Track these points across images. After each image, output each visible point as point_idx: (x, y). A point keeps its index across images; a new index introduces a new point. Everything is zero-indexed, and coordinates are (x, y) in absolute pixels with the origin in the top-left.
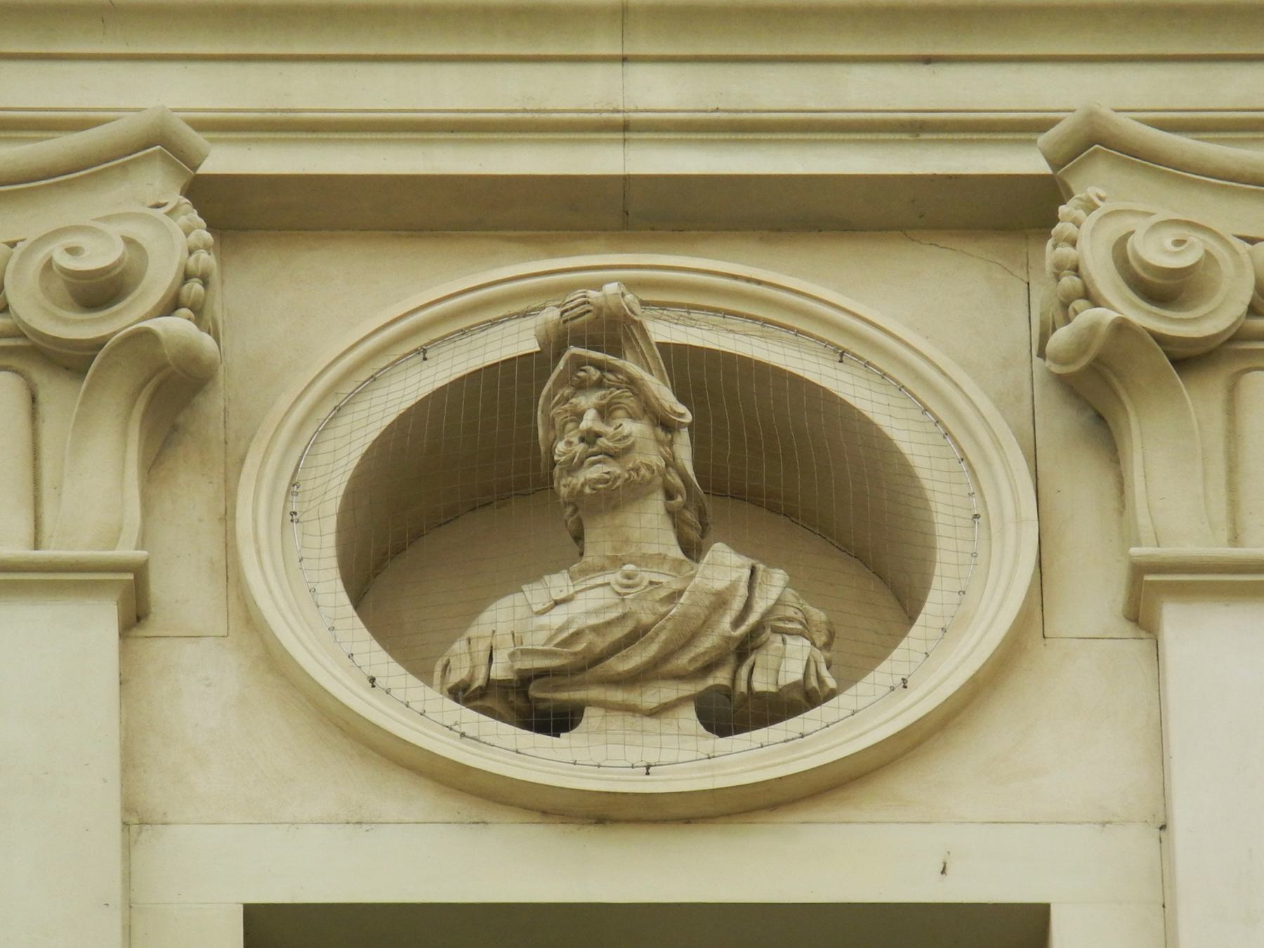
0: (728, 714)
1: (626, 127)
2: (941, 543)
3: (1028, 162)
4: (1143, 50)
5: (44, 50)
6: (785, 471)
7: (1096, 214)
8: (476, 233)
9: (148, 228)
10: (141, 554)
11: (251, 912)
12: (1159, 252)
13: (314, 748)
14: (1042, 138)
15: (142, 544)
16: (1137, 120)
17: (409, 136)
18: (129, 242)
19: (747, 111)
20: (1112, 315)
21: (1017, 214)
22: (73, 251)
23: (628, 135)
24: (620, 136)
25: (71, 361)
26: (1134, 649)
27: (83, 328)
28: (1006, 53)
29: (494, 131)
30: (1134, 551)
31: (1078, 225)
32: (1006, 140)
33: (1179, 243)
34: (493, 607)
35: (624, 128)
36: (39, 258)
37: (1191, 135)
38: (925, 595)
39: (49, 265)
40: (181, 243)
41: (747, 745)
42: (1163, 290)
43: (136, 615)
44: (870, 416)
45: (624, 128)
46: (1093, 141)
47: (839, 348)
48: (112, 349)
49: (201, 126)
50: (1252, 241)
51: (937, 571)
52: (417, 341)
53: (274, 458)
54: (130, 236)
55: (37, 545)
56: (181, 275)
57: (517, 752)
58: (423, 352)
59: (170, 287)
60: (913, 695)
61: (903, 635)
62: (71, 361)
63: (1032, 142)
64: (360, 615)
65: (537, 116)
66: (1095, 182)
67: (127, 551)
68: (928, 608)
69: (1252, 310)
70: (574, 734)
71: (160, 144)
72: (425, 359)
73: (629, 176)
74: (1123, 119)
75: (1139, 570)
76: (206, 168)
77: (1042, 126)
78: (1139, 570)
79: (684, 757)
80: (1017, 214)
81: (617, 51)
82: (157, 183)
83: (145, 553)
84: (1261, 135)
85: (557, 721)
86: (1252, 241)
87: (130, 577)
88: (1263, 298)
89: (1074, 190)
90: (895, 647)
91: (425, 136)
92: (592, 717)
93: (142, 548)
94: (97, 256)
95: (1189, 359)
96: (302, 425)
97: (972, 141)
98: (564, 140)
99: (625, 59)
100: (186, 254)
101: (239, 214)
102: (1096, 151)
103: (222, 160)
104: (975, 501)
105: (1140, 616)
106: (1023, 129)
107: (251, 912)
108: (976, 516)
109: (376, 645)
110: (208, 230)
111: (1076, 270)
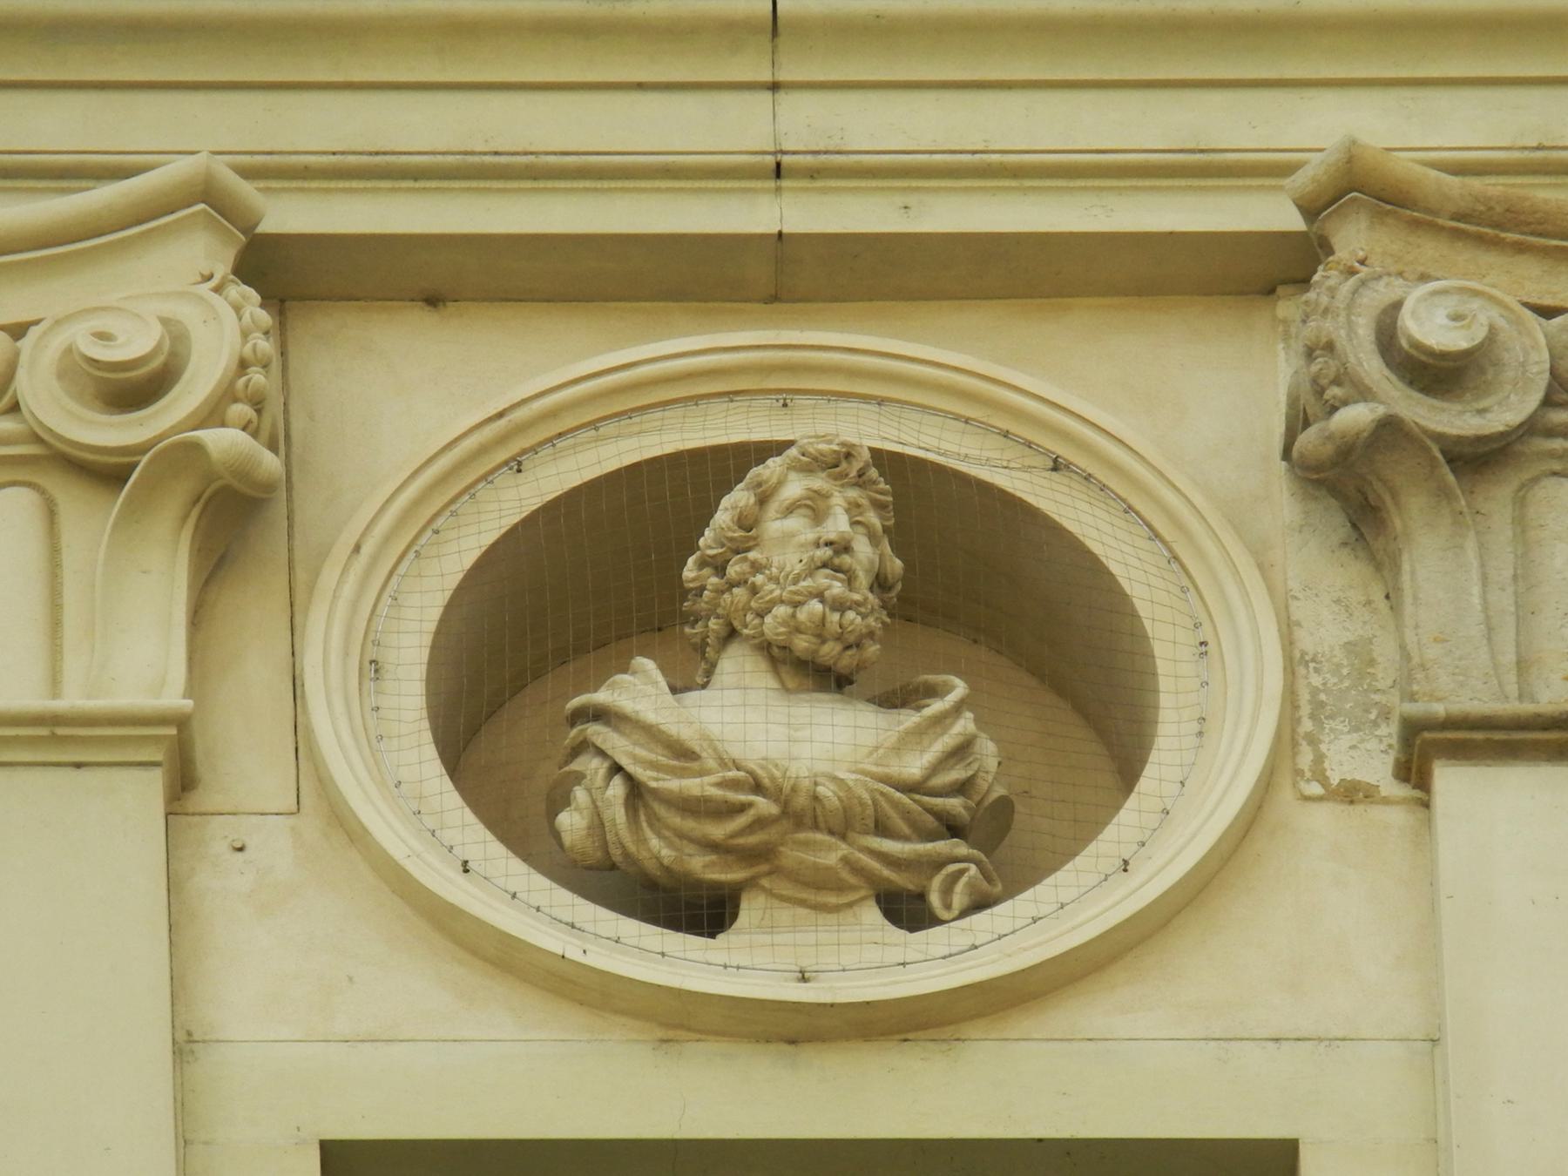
2: (1164, 683)
3: (1274, 214)
4: (1341, 73)
5: (1207, 76)
6: (984, 593)
8: (711, 305)
10: (188, 704)
12: (1433, 327)
13: (383, 938)
14: (1287, 182)
15: (189, 692)
18: (165, 322)
20: (1381, 410)
21: (1272, 272)
22: (103, 337)
25: (106, 473)
28: (1522, 74)
32: (1179, 188)
33: (1456, 317)
36: (58, 342)
39: (69, 351)
42: (1437, 374)
43: (183, 782)
46: (1357, 188)
50: (1547, 312)
52: (511, 443)
53: (348, 590)
54: (165, 315)
55: (55, 693)
56: (234, 366)
57: (573, 926)
59: (220, 382)
60: (1137, 875)
61: (1118, 808)
62: (106, 473)
63: (1281, 188)
65: (440, 158)
67: (173, 699)
69: (1548, 402)
72: (519, 471)
75: (1412, 730)
76: (267, 226)
77: (1285, 170)
78: (1412, 730)
79: (869, 961)
81: (766, 77)
82: (202, 252)
85: (707, 912)
86: (1547, 312)
87: (173, 731)
88: (1563, 388)
89: (1336, 247)
90: (1106, 824)
92: (751, 910)
94: (134, 342)
95: (1476, 460)
100: (238, 339)
102: (1354, 200)
103: (289, 215)
106: (1272, 171)
110: (262, 306)
111: (1330, 347)
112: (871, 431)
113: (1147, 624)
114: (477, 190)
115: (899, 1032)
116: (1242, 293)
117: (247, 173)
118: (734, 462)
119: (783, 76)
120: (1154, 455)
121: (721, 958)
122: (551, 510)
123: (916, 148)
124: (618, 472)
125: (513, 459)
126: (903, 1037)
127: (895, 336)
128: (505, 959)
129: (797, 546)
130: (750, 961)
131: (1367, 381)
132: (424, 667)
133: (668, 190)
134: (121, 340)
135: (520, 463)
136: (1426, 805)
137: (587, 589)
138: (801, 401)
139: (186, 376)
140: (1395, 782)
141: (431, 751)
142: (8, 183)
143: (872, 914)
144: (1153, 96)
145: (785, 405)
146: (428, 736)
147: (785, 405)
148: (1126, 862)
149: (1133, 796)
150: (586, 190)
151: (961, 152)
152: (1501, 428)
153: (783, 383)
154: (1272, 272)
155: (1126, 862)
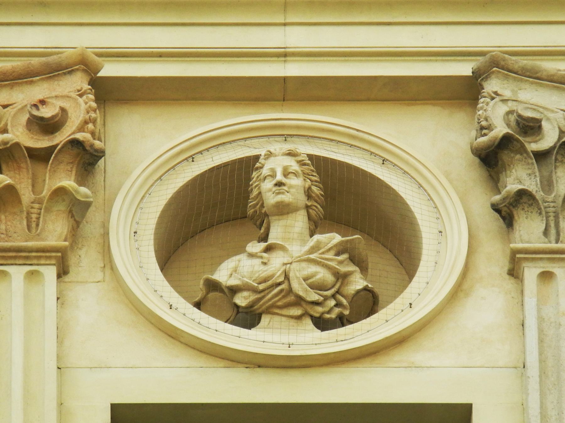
0: (322, 324)
1: (285, 55)
3: (464, 69)
6: (354, 206)
8: (204, 102)
9: (69, 98)
11: (115, 408)
21: (465, 93)
24: (283, 59)
25: (40, 156)
26: (509, 284)
27: (42, 143)
30: (512, 245)
31: (487, 104)
34: (227, 261)
35: (284, 55)
40: (83, 107)
44: (390, 184)
45: (284, 55)
47: (382, 157)
48: (60, 150)
49: (100, 55)
58: (192, 158)
60: (415, 309)
64: (165, 275)
65: (45, 50)
66: (492, 85)
68: (420, 269)
71: (85, 65)
72: (193, 161)
73: (287, 77)
75: (514, 252)
81: (283, 21)
82: (79, 81)
85: (248, 318)
87: (59, 254)
96: (147, 179)
99: (285, 24)
101: (110, 94)
103: (110, 70)
105: (514, 272)
107: (115, 408)
109: (172, 290)
112: (306, 149)
115: (246, 363)
116: (449, 99)
117: (100, 55)
119: (288, 21)
120: (424, 161)
123: (505, 45)
125: (191, 156)
126: (248, 366)
128: (173, 334)
130: (273, 337)
131: (57, 134)
132: (154, 230)
134: (25, 117)
135: (193, 158)
142: (2, 59)
144: (272, 28)
148: (411, 304)
150: (135, 61)
151: (519, 47)
152: (547, 148)
154: (465, 93)
155: (411, 304)
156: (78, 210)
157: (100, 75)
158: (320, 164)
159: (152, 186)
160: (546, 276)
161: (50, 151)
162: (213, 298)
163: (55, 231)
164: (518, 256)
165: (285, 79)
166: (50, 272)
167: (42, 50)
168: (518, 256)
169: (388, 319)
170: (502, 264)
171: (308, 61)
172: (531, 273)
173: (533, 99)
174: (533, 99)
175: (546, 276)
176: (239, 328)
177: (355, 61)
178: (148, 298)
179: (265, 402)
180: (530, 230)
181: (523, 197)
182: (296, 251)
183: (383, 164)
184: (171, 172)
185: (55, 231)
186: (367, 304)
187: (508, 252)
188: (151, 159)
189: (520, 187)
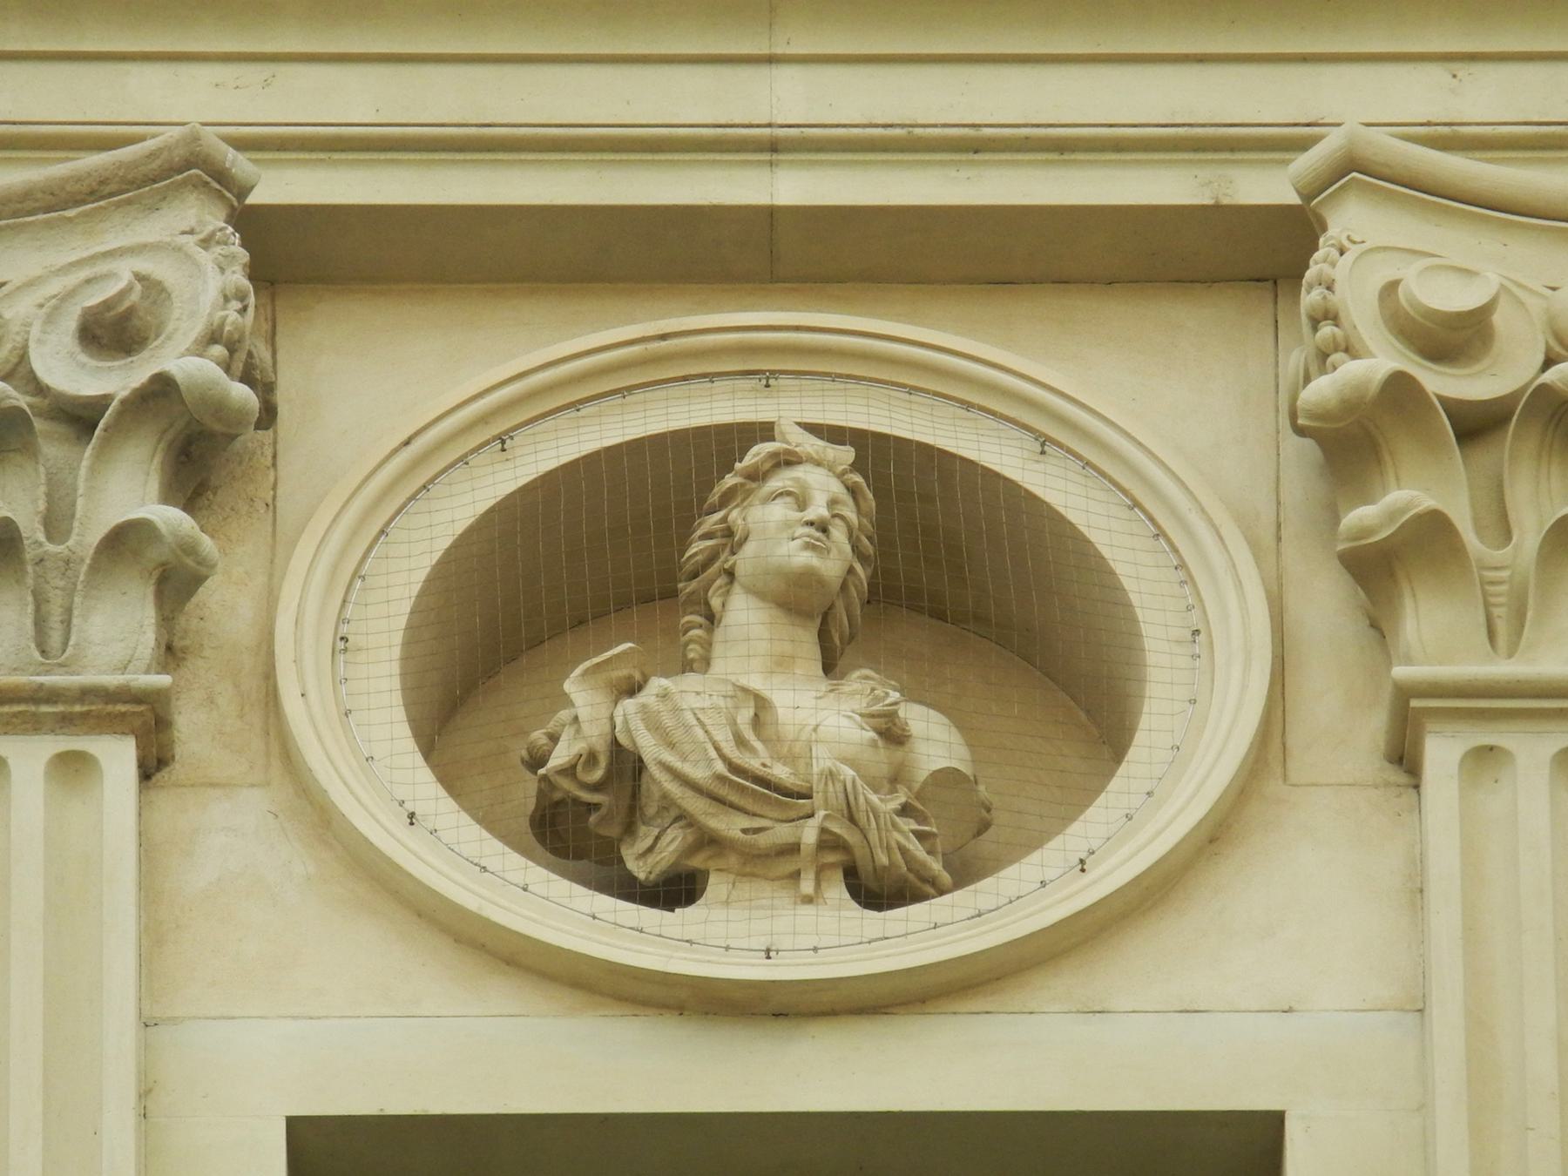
0: (878, 891)
1: (774, 146)
2: (1153, 674)
3: (1267, 186)
6: (961, 583)
7: (1349, 257)
9: (195, 275)
11: (297, 1128)
13: (353, 926)
16: (1392, 135)
17: (1210, 156)
19: (935, 126)
21: (1260, 259)
23: (775, 157)
24: (766, 157)
25: (80, 418)
29: (1003, 151)
30: (1400, 672)
35: (772, 147)
37: (1478, 155)
38: (1132, 737)
41: (900, 928)
44: (1062, 510)
45: (772, 147)
46: (1351, 169)
49: (241, 144)
50: (1554, 289)
51: (1146, 709)
65: (720, 131)
70: (689, 910)
71: (193, 169)
74: (1381, 137)
75: (1404, 694)
79: (828, 938)
80: (1260, 259)
81: (765, 51)
83: (164, 680)
84: (1564, 154)
86: (1554, 289)
91: (38, 154)
92: (716, 886)
93: (164, 668)
97: (379, 161)
98: (1157, 162)
101: (296, 258)
103: (277, 186)
104: (1195, 617)
107: (297, 1128)
108: (1196, 632)
113: (1138, 611)
114: (392, 161)
117: (241, 144)
118: (731, 441)
119: (779, 51)
120: (1148, 449)
121: (676, 932)
122: (548, 482)
124: (597, 454)
127: (881, 317)
129: (792, 524)
133: (354, 161)
134: (70, 323)
135: (503, 442)
136: (1417, 787)
137: (593, 562)
138: (784, 381)
139: (145, 354)
140: (1387, 764)
141: (404, 730)
142: (7, 154)
143: (837, 891)
145: (767, 386)
146: (400, 714)
147: (767, 386)
149: (1124, 764)
150: (1184, 161)
153: (760, 364)
156: (177, 583)
157: (253, 199)
158: (875, 456)
159: (398, 512)
160: (1484, 757)
161: (99, 405)
162: (581, 826)
163: (114, 638)
164: (1414, 703)
165: (771, 214)
166: (117, 756)
167: (473, 130)
168: (1414, 703)
169: (1047, 879)
170: (1374, 727)
171: (1190, 161)
172: (1442, 753)
173: (1454, 269)
174: (1454, 269)
175: (1484, 757)
176: (634, 906)
177: (1030, 163)
178: (378, 821)
179: (392, 1110)
180: (1438, 638)
181: (1429, 539)
182: (757, 695)
183: (1043, 453)
184: (456, 474)
185: (114, 638)
186: (960, 840)
187: (1386, 695)
188: (408, 436)
189: (9, 515)
